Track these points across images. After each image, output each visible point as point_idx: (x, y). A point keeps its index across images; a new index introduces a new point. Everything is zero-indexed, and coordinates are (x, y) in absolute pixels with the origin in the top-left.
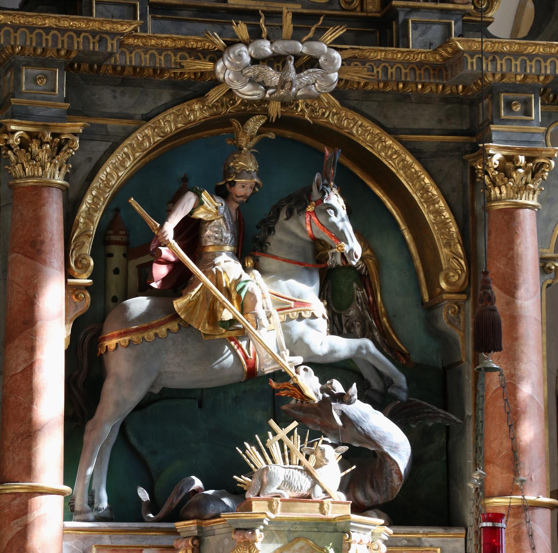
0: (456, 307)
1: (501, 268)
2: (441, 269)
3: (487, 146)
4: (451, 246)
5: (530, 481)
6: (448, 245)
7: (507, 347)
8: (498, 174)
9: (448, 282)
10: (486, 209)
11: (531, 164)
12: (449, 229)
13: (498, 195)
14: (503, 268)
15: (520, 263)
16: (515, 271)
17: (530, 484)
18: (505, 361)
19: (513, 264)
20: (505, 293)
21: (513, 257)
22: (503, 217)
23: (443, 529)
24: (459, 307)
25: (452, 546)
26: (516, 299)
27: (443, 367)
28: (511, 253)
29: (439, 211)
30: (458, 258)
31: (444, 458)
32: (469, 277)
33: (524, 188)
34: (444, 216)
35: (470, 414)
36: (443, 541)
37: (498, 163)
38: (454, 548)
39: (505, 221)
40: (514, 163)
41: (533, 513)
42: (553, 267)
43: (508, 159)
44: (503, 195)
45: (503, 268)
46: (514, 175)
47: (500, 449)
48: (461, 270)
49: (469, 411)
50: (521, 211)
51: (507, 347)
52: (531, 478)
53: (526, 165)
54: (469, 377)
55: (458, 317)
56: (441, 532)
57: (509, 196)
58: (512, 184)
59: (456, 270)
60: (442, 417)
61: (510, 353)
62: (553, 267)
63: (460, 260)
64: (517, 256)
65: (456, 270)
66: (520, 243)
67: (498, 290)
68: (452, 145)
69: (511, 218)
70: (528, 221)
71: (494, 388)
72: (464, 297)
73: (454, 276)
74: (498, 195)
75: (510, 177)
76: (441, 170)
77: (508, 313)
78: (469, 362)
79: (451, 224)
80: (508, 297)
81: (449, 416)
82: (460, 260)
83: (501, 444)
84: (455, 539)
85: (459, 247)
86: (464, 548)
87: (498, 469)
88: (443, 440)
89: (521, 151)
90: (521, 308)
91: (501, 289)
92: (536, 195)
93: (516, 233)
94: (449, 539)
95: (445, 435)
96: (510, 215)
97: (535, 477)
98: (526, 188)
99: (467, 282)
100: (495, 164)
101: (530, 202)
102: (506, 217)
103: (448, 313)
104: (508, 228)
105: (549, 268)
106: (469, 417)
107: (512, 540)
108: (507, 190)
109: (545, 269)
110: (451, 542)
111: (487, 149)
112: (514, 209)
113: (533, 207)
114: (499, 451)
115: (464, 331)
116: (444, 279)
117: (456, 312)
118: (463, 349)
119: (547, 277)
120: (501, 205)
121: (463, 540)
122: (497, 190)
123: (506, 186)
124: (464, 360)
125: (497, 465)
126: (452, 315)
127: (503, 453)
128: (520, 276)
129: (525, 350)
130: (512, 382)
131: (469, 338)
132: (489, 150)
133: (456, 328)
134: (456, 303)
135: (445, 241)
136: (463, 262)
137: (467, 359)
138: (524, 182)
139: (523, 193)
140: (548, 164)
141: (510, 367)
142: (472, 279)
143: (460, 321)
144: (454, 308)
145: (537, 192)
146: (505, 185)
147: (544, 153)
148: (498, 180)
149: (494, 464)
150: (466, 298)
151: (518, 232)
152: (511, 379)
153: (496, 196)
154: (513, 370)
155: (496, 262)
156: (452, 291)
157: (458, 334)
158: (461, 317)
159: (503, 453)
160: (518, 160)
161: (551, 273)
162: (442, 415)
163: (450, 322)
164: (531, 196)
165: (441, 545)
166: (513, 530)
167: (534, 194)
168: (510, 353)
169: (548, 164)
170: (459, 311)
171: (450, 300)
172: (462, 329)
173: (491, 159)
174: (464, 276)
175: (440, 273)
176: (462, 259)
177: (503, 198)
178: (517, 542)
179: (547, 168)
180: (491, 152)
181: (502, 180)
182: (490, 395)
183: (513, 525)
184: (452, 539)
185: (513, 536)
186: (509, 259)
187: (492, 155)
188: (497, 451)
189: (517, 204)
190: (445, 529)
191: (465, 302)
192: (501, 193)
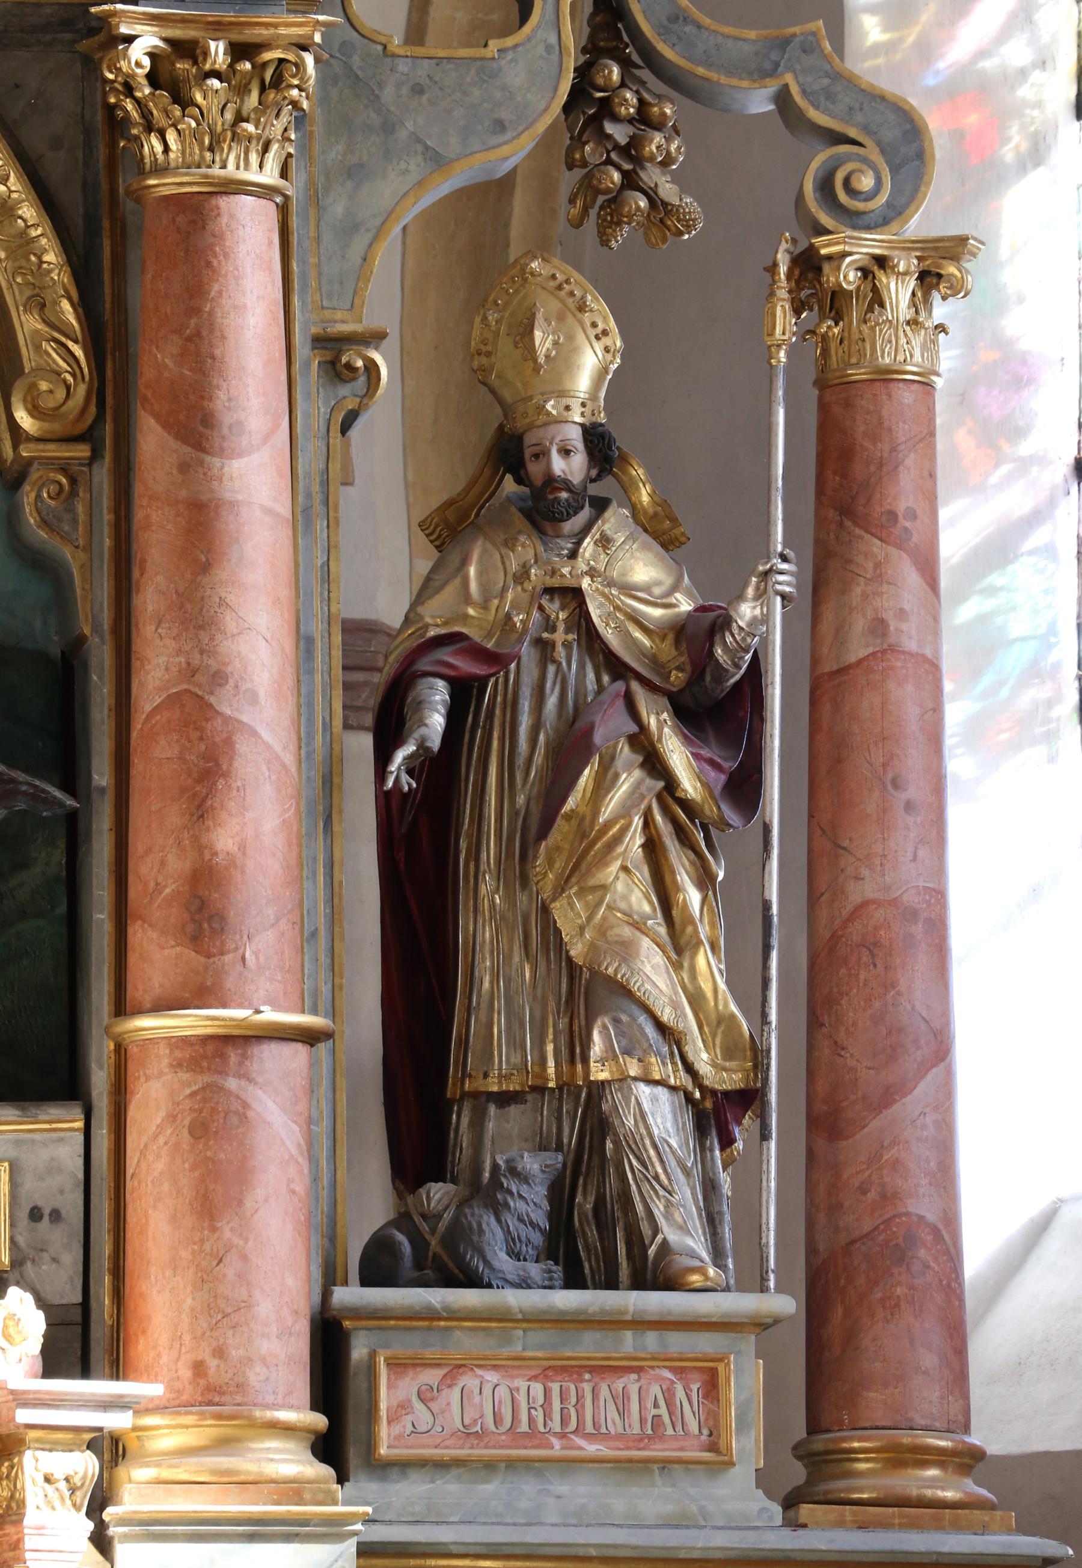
0: (64, 481)
1: (166, 366)
2: (19, 371)
3: (114, 14)
4: (43, 305)
5: (239, 967)
6: (40, 304)
7: (181, 589)
8: (152, 94)
9: (35, 411)
10: (138, 196)
11: (248, 66)
12: (39, 258)
13: (160, 157)
14: (171, 365)
15: (217, 352)
16: (204, 374)
17: (240, 974)
18: (175, 631)
19: (198, 353)
20: (177, 436)
21: (198, 334)
22: (174, 221)
23: (17, 1108)
24: (73, 481)
25: (44, 1155)
26: (221, 453)
27: (63, 653)
28: (193, 322)
29: (10, 203)
30: (63, 339)
31: (62, 909)
32: (98, 393)
33: (229, 134)
34: (25, 221)
35: (104, 783)
36: (18, 1143)
37: (146, 62)
38: (52, 1159)
39: (179, 232)
40: (195, 62)
41: (245, 1056)
42: (360, 363)
43: (187, 49)
44: (172, 155)
45: (171, 365)
46: (199, 98)
47: (160, 880)
48: (74, 375)
49: (102, 775)
50: (223, 202)
51: (181, 589)
52: (243, 959)
53: (231, 66)
54: (100, 678)
55: (71, 510)
56: (9, 1119)
57: (188, 159)
58: (194, 124)
59: (59, 374)
60: (25, 793)
61: (188, 606)
62: (360, 363)
63: (70, 344)
64: (211, 331)
65: (59, 374)
66: (220, 292)
67: (159, 429)
68: (48, 11)
69: (194, 222)
70: (249, 235)
71: (148, 707)
72: (82, 451)
73: (51, 391)
74: (160, 157)
75: (183, 101)
76: (17, 86)
77: (183, 493)
78: (102, 638)
79: (44, 241)
80: (187, 449)
81: (44, 791)
82: (70, 344)
83: (163, 863)
84: (54, 1135)
85: (66, 305)
86: (80, 1162)
87: (154, 935)
88: (59, 856)
89: (217, 28)
90: (220, 479)
91: (166, 426)
92: (270, 156)
93: (209, 264)
94: (37, 1136)
95: (62, 844)
96: (195, 214)
97: (256, 954)
98: (234, 134)
99: (93, 409)
100: (138, 64)
101: (253, 176)
102: (181, 219)
103: (39, 496)
104: (186, 251)
105: (349, 367)
106: (102, 791)
107: (185, 1131)
108: (183, 143)
109: (338, 367)
110: (44, 1144)
111: (114, 21)
112: (201, 197)
113: (265, 192)
114: (157, 884)
115: (88, 548)
116: (25, 401)
117: (63, 496)
118: (84, 598)
119: (344, 390)
120: (161, 186)
121: (80, 1138)
122: (155, 140)
123: (178, 131)
124: (87, 631)
125: (150, 926)
126: (52, 503)
127: (167, 891)
128: (218, 387)
129: (231, 599)
130: (193, 689)
131: (102, 567)
132: (117, 26)
133: (66, 538)
134: (64, 471)
135: (28, 293)
136: (78, 351)
137: (96, 629)
138: (229, 116)
139: (230, 148)
140: (296, 65)
141: (187, 648)
142: (109, 401)
143: (75, 521)
144: (59, 483)
145: (275, 147)
146: (174, 125)
147: (282, 31)
148: (155, 112)
149: (144, 922)
150: (88, 454)
151: (215, 263)
152: (189, 682)
153: (156, 160)
154: (197, 656)
155: (155, 350)
156: (54, 437)
157: (71, 557)
158: (80, 509)
159: (167, 891)
160: (206, 53)
161: (354, 379)
162: (24, 788)
163: (44, 523)
164: (254, 158)
165: (12, 1153)
166: (188, 1104)
167: (266, 149)
168: (188, 606)
169: (296, 65)
170: (73, 493)
171: (48, 462)
172: (81, 542)
173: (126, 49)
174: (82, 389)
175: (15, 380)
176: (76, 341)
177: (173, 164)
178: (196, 1138)
179: (293, 76)
180: (124, 30)
181: (167, 113)
182: (139, 726)
183: (188, 1091)
184: (46, 1135)
185: (187, 1122)
186: (189, 339)
187: (130, 39)
188: (152, 884)
189: (207, 180)
190: (23, 1109)
191: (90, 465)
192: (166, 149)
